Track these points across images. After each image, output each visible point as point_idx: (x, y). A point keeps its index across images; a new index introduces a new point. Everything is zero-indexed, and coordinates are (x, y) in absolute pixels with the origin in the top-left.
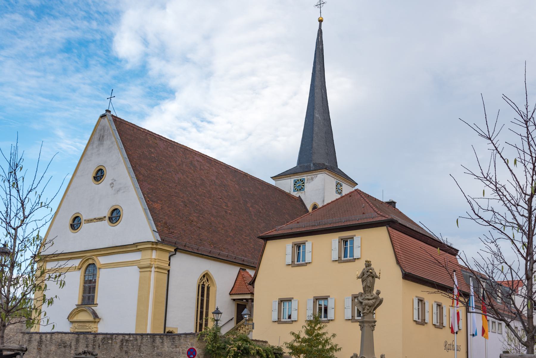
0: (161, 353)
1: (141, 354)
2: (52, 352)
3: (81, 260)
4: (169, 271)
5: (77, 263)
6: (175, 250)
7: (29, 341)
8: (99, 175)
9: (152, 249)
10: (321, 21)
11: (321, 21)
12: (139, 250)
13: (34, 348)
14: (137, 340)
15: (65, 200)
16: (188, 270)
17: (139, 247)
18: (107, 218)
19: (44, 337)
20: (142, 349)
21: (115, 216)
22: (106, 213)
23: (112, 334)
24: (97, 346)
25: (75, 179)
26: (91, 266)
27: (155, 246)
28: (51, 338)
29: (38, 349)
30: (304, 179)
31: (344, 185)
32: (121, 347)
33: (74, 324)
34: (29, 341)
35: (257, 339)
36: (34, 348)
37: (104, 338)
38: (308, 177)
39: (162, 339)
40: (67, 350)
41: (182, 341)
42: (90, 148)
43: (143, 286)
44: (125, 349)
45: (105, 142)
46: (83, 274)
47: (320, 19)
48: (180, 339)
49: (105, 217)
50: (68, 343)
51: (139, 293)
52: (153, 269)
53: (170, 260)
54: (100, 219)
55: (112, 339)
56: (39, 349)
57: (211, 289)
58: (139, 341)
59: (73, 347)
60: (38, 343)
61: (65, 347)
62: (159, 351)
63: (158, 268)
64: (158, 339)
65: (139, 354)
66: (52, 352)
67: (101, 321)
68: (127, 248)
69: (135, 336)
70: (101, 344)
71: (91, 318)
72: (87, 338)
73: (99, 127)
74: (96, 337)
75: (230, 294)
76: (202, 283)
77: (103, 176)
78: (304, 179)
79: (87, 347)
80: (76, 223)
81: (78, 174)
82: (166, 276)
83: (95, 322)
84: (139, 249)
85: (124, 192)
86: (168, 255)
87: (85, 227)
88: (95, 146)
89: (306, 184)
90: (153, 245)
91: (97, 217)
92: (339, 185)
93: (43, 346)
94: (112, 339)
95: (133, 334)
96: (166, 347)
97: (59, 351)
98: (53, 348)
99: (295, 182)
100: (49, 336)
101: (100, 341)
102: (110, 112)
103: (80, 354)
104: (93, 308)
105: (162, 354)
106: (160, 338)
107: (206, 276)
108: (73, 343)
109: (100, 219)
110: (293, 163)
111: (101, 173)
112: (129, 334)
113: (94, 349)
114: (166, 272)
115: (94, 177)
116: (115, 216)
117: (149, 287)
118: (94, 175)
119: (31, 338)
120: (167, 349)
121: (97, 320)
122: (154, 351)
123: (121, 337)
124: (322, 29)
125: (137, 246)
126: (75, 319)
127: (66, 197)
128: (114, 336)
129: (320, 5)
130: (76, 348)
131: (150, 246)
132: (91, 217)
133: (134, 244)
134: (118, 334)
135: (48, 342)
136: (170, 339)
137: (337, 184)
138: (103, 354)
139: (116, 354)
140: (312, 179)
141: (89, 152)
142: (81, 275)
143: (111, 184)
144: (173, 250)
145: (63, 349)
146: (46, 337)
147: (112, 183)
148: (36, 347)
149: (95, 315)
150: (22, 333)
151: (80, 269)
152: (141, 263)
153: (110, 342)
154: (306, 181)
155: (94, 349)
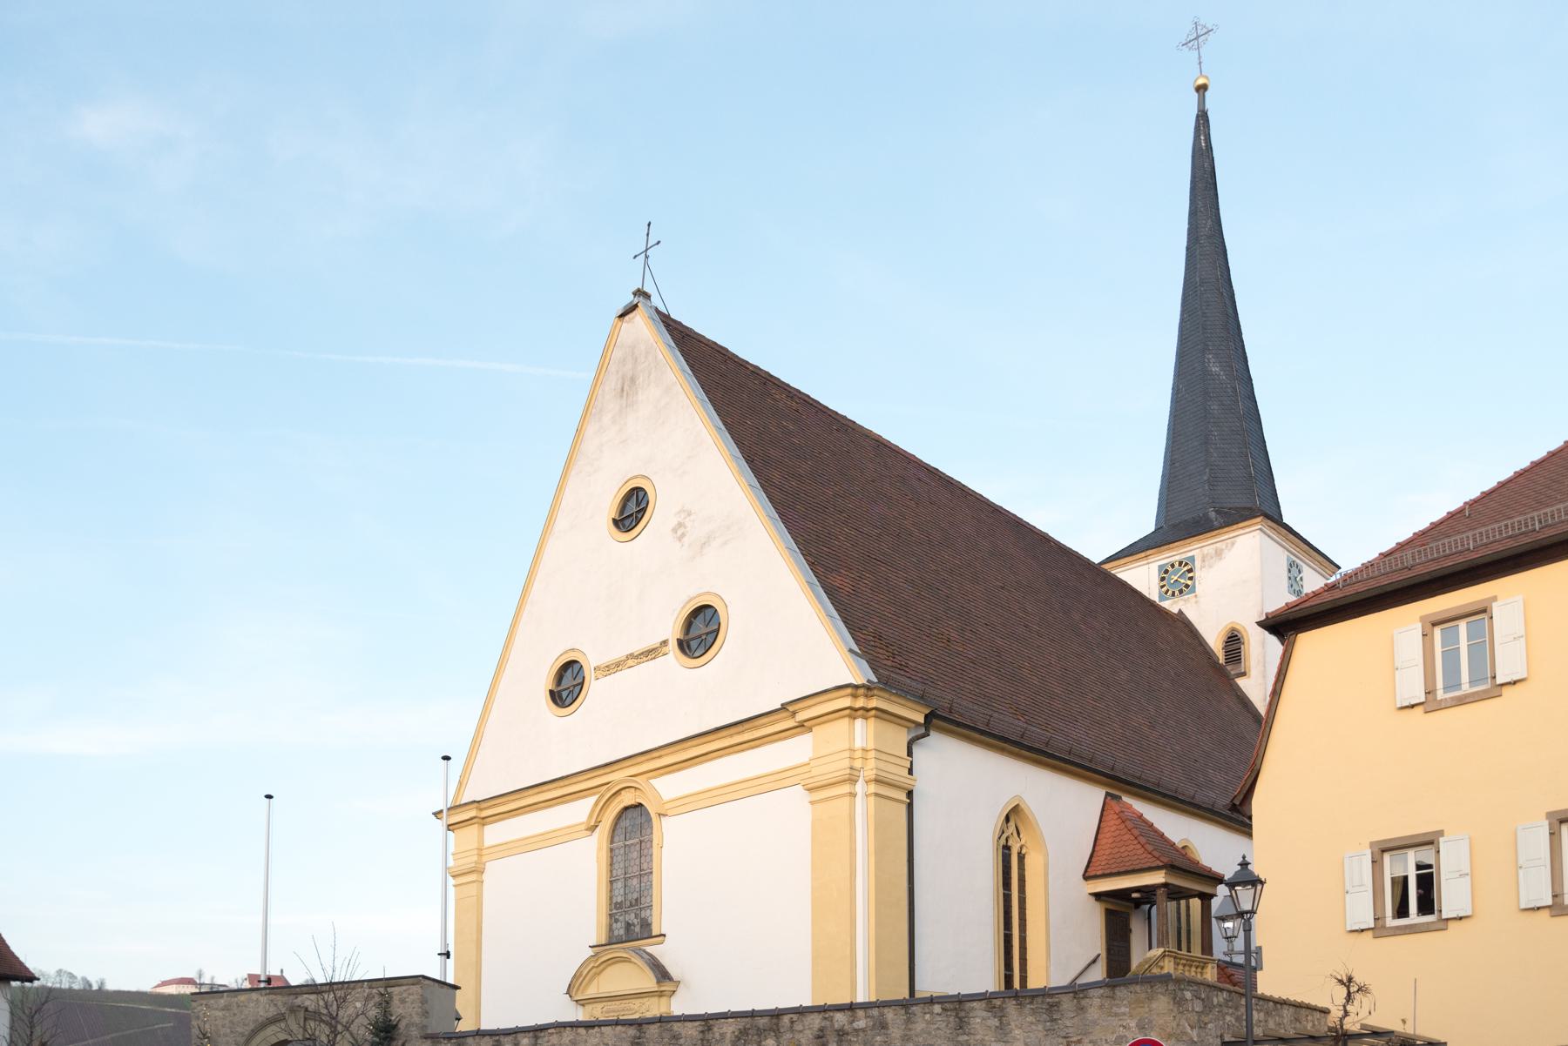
3: (593, 799)
4: (910, 794)
5: (581, 810)
6: (926, 717)
8: (632, 510)
9: (853, 713)
10: (1202, 89)
11: (1202, 89)
12: (803, 727)
14: (883, 1026)
15: (525, 618)
16: (968, 784)
17: (801, 716)
18: (673, 645)
21: (700, 631)
22: (670, 628)
23: (776, 1014)
25: (552, 545)
26: (630, 813)
27: (860, 703)
30: (1192, 559)
31: (1305, 569)
33: (589, 1007)
35: (1313, 1003)
37: (744, 1032)
38: (1206, 550)
39: (1000, 1013)
41: (1093, 1013)
42: (590, 430)
46: (605, 845)
47: (1201, 81)
48: (1081, 1009)
49: (665, 643)
52: (859, 788)
53: (910, 754)
54: (650, 654)
57: (1027, 861)
58: (896, 1032)
63: (878, 781)
64: (979, 1017)
67: (681, 991)
68: (757, 728)
69: (875, 1012)
71: (648, 982)
73: (617, 354)
74: (710, 1029)
75: (1086, 877)
76: (1003, 841)
77: (644, 510)
78: (1192, 559)
80: (567, 685)
81: (561, 522)
82: (904, 808)
83: (661, 994)
84: (801, 725)
85: (725, 543)
86: (903, 737)
87: (596, 690)
89: (1197, 574)
90: (855, 696)
91: (637, 648)
92: (1294, 569)
95: (866, 1006)
99: (1165, 572)
102: (647, 296)
104: (649, 949)
107: (1014, 815)
109: (650, 654)
110: (1146, 525)
111: (638, 504)
112: (851, 1008)
115: (616, 522)
116: (700, 631)
117: (853, 852)
118: (614, 514)
121: (667, 987)
123: (816, 1021)
124: (1208, 106)
125: (794, 713)
126: (592, 992)
128: (786, 1019)
129: (1197, 38)
132: (618, 653)
133: (784, 707)
134: (801, 1011)
136: (1034, 1012)
137: (1291, 565)
140: (1219, 554)
141: (589, 445)
142: (599, 849)
143: (675, 530)
144: (921, 719)
147: (680, 525)
149: (662, 974)
150: (426, 1037)
152: (815, 772)
154: (1198, 564)
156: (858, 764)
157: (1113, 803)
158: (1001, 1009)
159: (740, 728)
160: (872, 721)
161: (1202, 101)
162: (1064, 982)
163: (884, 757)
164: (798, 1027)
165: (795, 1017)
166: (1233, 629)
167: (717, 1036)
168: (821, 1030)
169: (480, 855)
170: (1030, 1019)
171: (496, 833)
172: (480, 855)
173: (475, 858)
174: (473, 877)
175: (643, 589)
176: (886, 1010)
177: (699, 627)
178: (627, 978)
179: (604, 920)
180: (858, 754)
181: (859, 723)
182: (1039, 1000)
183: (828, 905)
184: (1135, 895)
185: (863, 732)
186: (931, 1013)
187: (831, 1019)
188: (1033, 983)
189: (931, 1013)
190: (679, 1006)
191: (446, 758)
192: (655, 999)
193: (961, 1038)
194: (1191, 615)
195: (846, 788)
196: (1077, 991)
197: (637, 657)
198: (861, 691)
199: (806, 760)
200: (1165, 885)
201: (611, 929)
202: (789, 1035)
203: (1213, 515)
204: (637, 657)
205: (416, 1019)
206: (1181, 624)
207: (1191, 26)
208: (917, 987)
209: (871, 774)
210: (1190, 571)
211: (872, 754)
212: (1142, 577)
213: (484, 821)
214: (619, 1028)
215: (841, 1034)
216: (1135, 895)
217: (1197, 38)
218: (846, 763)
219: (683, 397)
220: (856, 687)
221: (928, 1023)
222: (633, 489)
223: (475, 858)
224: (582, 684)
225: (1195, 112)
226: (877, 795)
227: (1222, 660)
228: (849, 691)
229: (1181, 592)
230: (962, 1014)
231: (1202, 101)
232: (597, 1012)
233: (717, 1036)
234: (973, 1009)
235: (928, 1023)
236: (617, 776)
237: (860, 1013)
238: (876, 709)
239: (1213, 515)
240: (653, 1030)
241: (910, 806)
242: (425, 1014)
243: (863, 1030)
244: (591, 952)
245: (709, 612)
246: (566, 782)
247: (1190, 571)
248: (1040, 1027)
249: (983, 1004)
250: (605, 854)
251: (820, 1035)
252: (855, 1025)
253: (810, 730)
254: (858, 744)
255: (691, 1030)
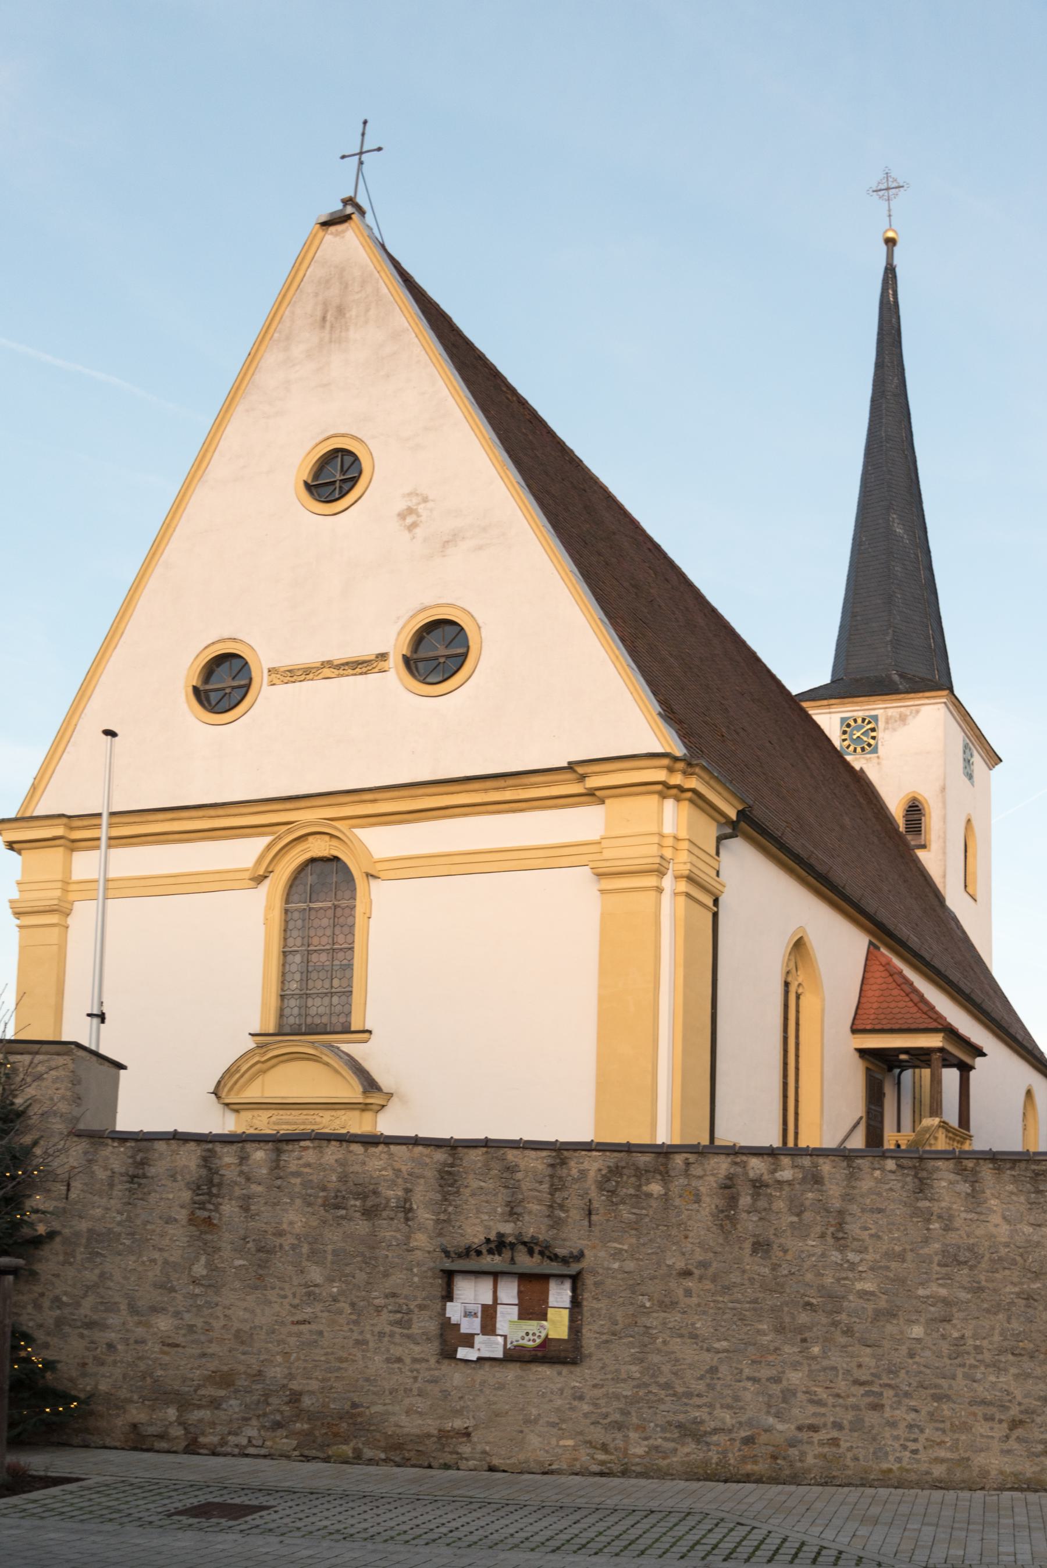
0: (970, 1249)
1: (851, 1256)
2: (288, 1241)
4: (716, 902)
5: (246, 852)
7: (132, 1178)
8: (335, 476)
9: (665, 790)
10: (890, 242)
11: (890, 242)
12: (593, 796)
13: (170, 1220)
14: (817, 1180)
15: (153, 583)
17: (592, 782)
18: (395, 662)
19: (228, 1157)
20: (853, 1228)
21: (438, 651)
22: (392, 638)
24: (576, 1215)
25: (201, 496)
27: (677, 779)
28: (276, 1165)
29: (192, 1221)
30: (875, 718)
32: (727, 1214)
33: (246, 1115)
34: (132, 1178)
36: (170, 1220)
37: (615, 1171)
38: (890, 712)
40: (389, 1231)
42: (271, 358)
43: (620, 957)
44: (748, 1223)
45: (353, 334)
47: (890, 234)
49: (383, 656)
50: (393, 1194)
51: (601, 986)
52: (667, 882)
54: (358, 666)
55: (665, 1176)
56: (203, 1223)
58: (834, 1190)
59: (424, 1216)
60: (197, 1189)
61: (370, 1213)
62: (952, 1238)
65: (836, 1256)
66: (288, 1241)
67: (394, 1106)
68: (525, 786)
69: (806, 1161)
70: (599, 1201)
71: (351, 1091)
72: (511, 1169)
73: (315, 272)
74: (563, 1162)
75: (854, 1031)
77: (354, 481)
78: (875, 718)
79: (513, 1212)
80: (223, 683)
81: (219, 468)
83: (365, 1107)
85: (480, 548)
87: (267, 700)
88: (297, 351)
89: (880, 734)
90: (671, 770)
93: (229, 1209)
94: (665, 1176)
96: (995, 1218)
97: (333, 1238)
98: (295, 1218)
100: (259, 1155)
101: (590, 1184)
103: (1009, 1269)
104: (345, 1047)
105: (979, 1257)
106: (961, 1171)
108: (423, 1196)
109: (358, 666)
113: (557, 1224)
114: (710, 902)
116: (438, 651)
118: (306, 474)
119: (143, 1163)
120: (1005, 1228)
121: (375, 1100)
122: (926, 1241)
124: (896, 262)
125: (582, 778)
126: (253, 1093)
127: (159, 571)
128: (679, 1160)
129: (888, 189)
130: (443, 1224)
131: (661, 775)
133: (571, 767)
135: (256, 1189)
136: (1015, 1179)
138: (617, 1255)
139: (699, 1256)
140: (903, 719)
142: (269, 908)
143: (402, 516)
145: (361, 1227)
146: (243, 1159)
147: (410, 511)
148: (182, 1215)
149: (370, 1084)
150: (80, 1135)
151: (260, 879)
152: (607, 854)
153: (655, 1188)
154: (881, 724)
155: (557, 1224)
156: (668, 853)
157: (875, 952)
158: (974, 1172)
159: (501, 783)
160: (685, 805)
161: (890, 255)
162: (833, 1144)
163: (696, 851)
164: (697, 1171)
165: (692, 1158)
166: (915, 799)
167: (574, 1172)
168: (730, 1177)
169: (66, 891)
170: (1011, 1187)
171: (85, 865)
172: (66, 891)
173: (58, 893)
174: (53, 919)
175: (367, 577)
176: (821, 1160)
177: (223, 680)
178: (304, 1083)
179: (273, 1002)
180: (669, 842)
181: (669, 804)
182: (1023, 1165)
183: (619, 1019)
184: (903, 1057)
185: (673, 817)
186: (882, 1169)
187: (744, 1165)
188: (802, 1144)
189: (882, 1169)
190: (387, 1124)
191: (110, 733)
192: (356, 1114)
193: (920, 1204)
194: (873, 775)
195: (651, 881)
196: (842, 1154)
197: (338, 667)
198: (681, 765)
199: (597, 838)
200: (941, 1050)
201: (281, 1015)
202: (682, 1181)
203: (896, 678)
204: (338, 667)
205: (63, 1107)
206: (860, 782)
207: (881, 175)
208: (717, 1134)
209: (685, 869)
210: (873, 730)
211: (685, 845)
212: (829, 720)
213: (74, 845)
214: (420, 1148)
215: (758, 1185)
216: (903, 1057)
217: (888, 189)
218: (654, 850)
219: (417, 351)
220: (676, 759)
221: (878, 1181)
222: (337, 451)
223: (58, 893)
224: (248, 687)
225: (883, 264)
226: (688, 895)
227: (902, 828)
228: (666, 762)
229: (863, 749)
230: (924, 1174)
231: (890, 255)
232: (263, 1123)
233: (574, 1172)
234: (938, 1169)
235: (878, 1181)
236: (307, 816)
237: (786, 1161)
238: (694, 791)
239: (896, 678)
240: (475, 1156)
241: (715, 915)
242: (77, 1099)
243: (789, 1183)
244: (250, 1044)
245: (237, 664)
246: (220, 811)
247: (873, 730)
248: (1022, 1199)
249: (951, 1164)
250: (277, 915)
251: (728, 1185)
252: (779, 1175)
253: (603, 802)
254: (668, 829)
255: (536, 1162)
